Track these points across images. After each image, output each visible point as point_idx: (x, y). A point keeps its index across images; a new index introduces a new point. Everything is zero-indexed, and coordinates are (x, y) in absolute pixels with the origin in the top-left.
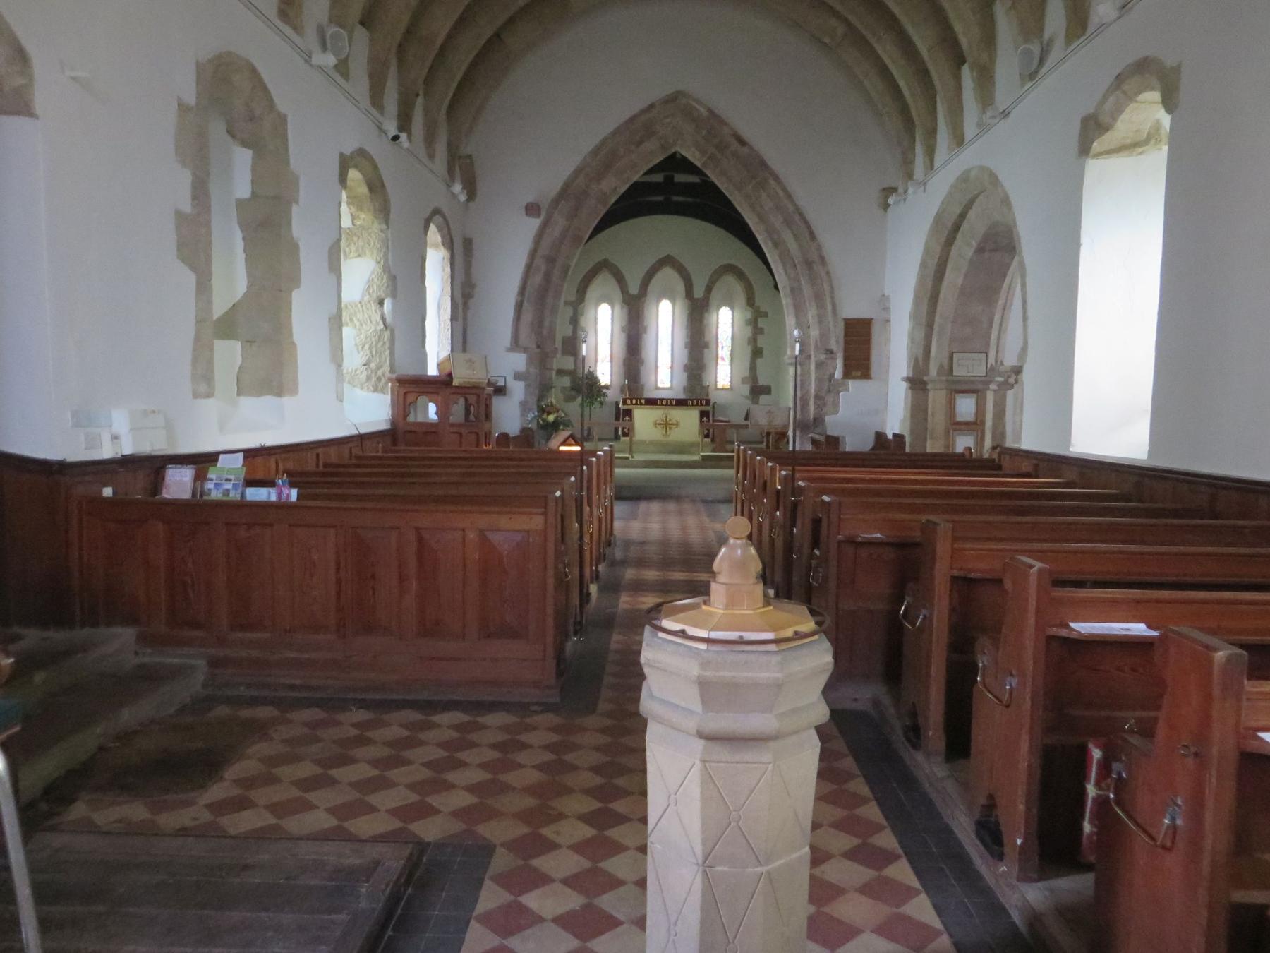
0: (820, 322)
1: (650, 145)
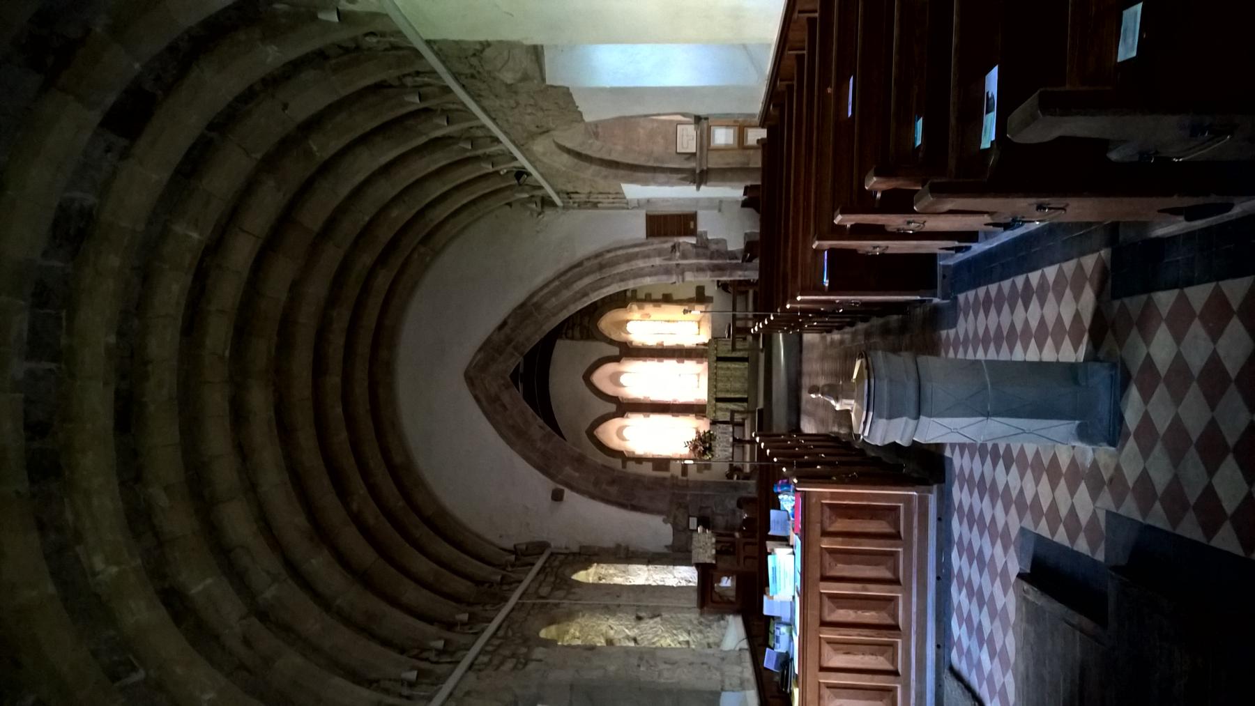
1: (506, 398)
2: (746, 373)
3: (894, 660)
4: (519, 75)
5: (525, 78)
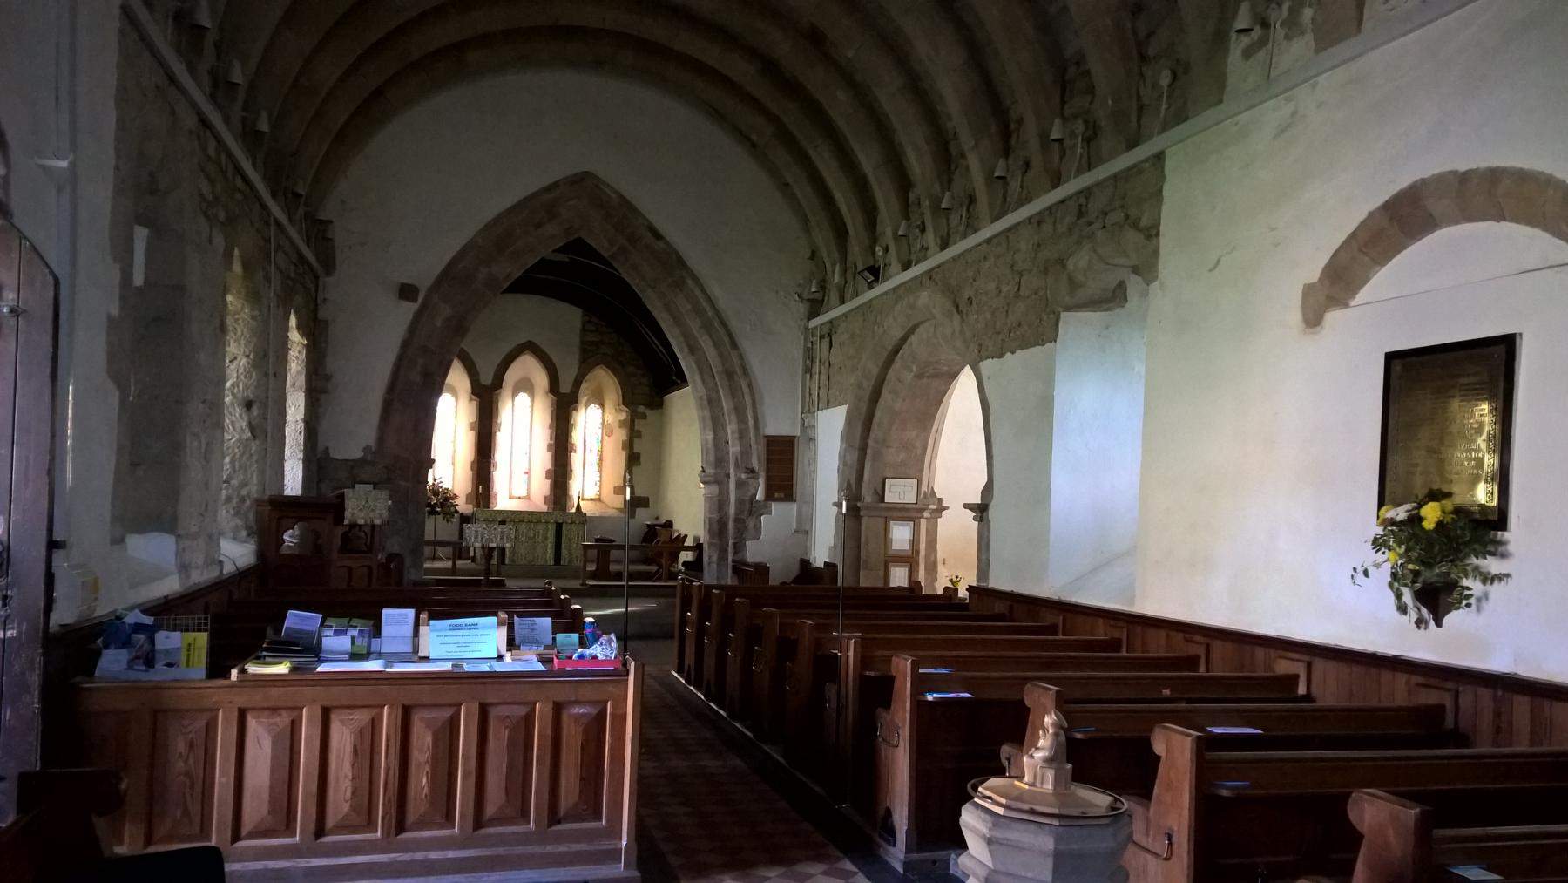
0: (741, 438)
2: (540, 562)
3: (342, 828)
4: (1079, 277)
5: (1073, 285)
